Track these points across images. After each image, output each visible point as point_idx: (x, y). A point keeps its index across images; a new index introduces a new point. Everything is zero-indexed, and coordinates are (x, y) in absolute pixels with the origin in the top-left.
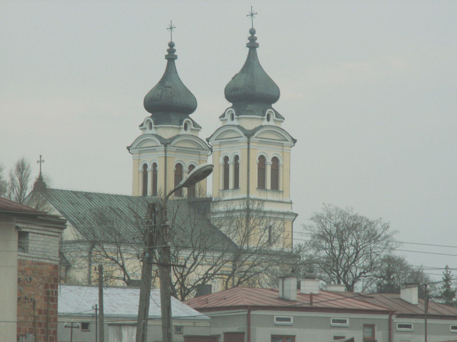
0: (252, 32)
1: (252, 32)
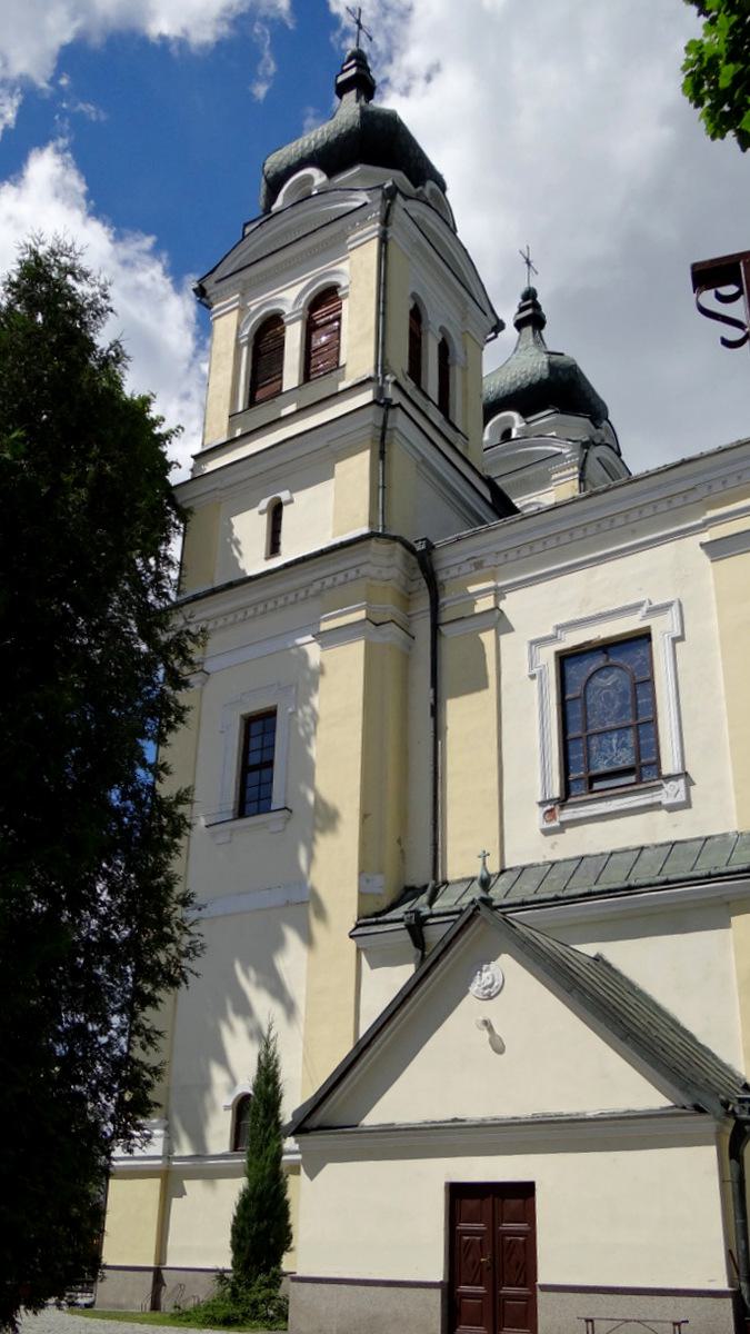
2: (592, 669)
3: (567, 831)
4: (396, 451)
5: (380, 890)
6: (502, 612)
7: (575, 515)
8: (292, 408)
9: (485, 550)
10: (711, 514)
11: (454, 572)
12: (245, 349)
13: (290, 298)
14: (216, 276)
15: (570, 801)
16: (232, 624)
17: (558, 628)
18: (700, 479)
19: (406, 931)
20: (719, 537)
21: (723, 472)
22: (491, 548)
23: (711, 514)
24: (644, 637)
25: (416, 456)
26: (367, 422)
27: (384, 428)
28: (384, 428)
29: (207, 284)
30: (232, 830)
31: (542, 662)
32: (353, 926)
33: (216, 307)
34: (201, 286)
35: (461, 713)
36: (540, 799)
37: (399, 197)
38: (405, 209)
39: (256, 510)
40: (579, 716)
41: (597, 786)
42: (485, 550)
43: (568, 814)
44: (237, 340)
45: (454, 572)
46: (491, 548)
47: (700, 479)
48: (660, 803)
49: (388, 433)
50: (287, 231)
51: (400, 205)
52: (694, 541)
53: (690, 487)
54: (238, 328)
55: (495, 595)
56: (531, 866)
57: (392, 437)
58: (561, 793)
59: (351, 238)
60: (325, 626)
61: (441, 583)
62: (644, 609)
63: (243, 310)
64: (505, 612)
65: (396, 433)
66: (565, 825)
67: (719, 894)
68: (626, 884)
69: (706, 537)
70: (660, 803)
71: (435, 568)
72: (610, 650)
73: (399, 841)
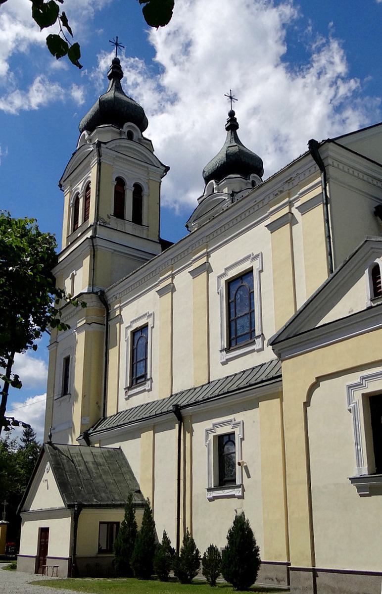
0: (232, 114)
1: (232, 114)
2: (237, 287)
3: (229, 363)
4: (99, 254)
5: (88, 423)
6: (292, 214)
7: (142, 274)
8: (80, 234)
9: (116, 293)
10: (271, 209)
11: (111, 301)
12: (72, 209)
13: (80, 187)
14: (63, 179)
15: (231, 348)
16: (70, 318)
17: (131, 322)
18: (264, 195)
19: (83, 440)
20: (305, 201)
21: (200, 238)
22: (118, 292)
23: (271, 209)
24: (250, 272)
25: (111, 250)
26: (87, 246)
27: (93, 246)
28: (93, 246)
29: (62, 183)
30: (60, 402)
31: (222, 286)
32: (79, 436)
33: (65, 191)
34: (60, 184)
35: (113, 353)
36: (125, 387)
37: (102, 145)
38: (107, 148)
39: (69, 278)
40: (233, 310)
41: (139, 381)
42: (116, 293)
43: (131, 392)
44: (69, 205)
45: (111, 301)
46: (118, 292)
47: (264, 195)
48: (145, 389)
49: (95, 247)
50: (79, 159)
51: (104, 148)
52: (153, 292)
53: (262, 199)
54: (70, 200)
55: (207, 256)
56: (247, 370)
57: (97, 248)
58: (227, 346)
59: (92, 163)
60: (79, 325)
61: (110, 305)
62: (251, 258)
63: (71, 192)
64: (294, 214)
65: (98, 247)
66: (130, 396)
67: (137, 427)
68: (129, 421)
69: (158, 288)
70: (145, 389)
71: (322, 157)
72: (243, 278)
73: (97, 403)
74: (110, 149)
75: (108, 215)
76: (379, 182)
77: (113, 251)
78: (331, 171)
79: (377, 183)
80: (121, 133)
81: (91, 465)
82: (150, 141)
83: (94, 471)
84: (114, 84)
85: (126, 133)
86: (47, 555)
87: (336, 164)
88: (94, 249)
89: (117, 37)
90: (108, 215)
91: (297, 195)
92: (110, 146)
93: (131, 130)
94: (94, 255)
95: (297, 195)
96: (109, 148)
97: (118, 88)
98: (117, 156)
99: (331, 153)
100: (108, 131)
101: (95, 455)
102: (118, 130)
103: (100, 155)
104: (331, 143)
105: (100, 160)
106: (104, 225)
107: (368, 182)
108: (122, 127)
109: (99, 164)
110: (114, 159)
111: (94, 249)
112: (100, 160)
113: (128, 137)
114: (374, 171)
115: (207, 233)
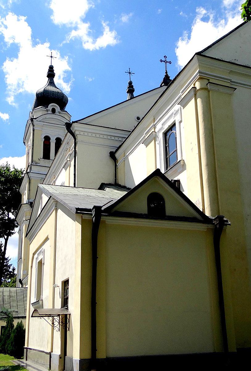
0: (130, 83)
1: (130, 83)
4: (32, 181)
27: (29, 177)
28: (29, 177)
74: (39, 121)
75: (38, 159)
76: (119, 138)
77: (41, 179)
78: (79, 138)
79: (118, 138)
80: (47, 111)
81: (6, 298)
82: (66, 112)
83: (6, 300)
84: (49, 81)
85: (51, 110)
86: (24, 346)
87: (82, 133)
88: (29, 178)
89: (129, 68)
90: (38, 159)
91: (144, 135)
92: (39, 119)
93: (53, 107)
94: (30, 182)
95: (144, 135)
96: (39, 120)
97: (51, 83)
98: (43, 125)
99: (76, 128)
100: (40, 111)
101: (11, 292)
102: (46, 109)
103: (34, 126)
104: (75, 123)
105: (34, 128)
106: (36, 164)
107: (108, 139)
108: (47, 107)
109: (34, 130)
110: (42, 126)
111: (29, 178)
112: (34, 128)
113: (52, 112)
114: (110, 132)
115: (53, 171)
